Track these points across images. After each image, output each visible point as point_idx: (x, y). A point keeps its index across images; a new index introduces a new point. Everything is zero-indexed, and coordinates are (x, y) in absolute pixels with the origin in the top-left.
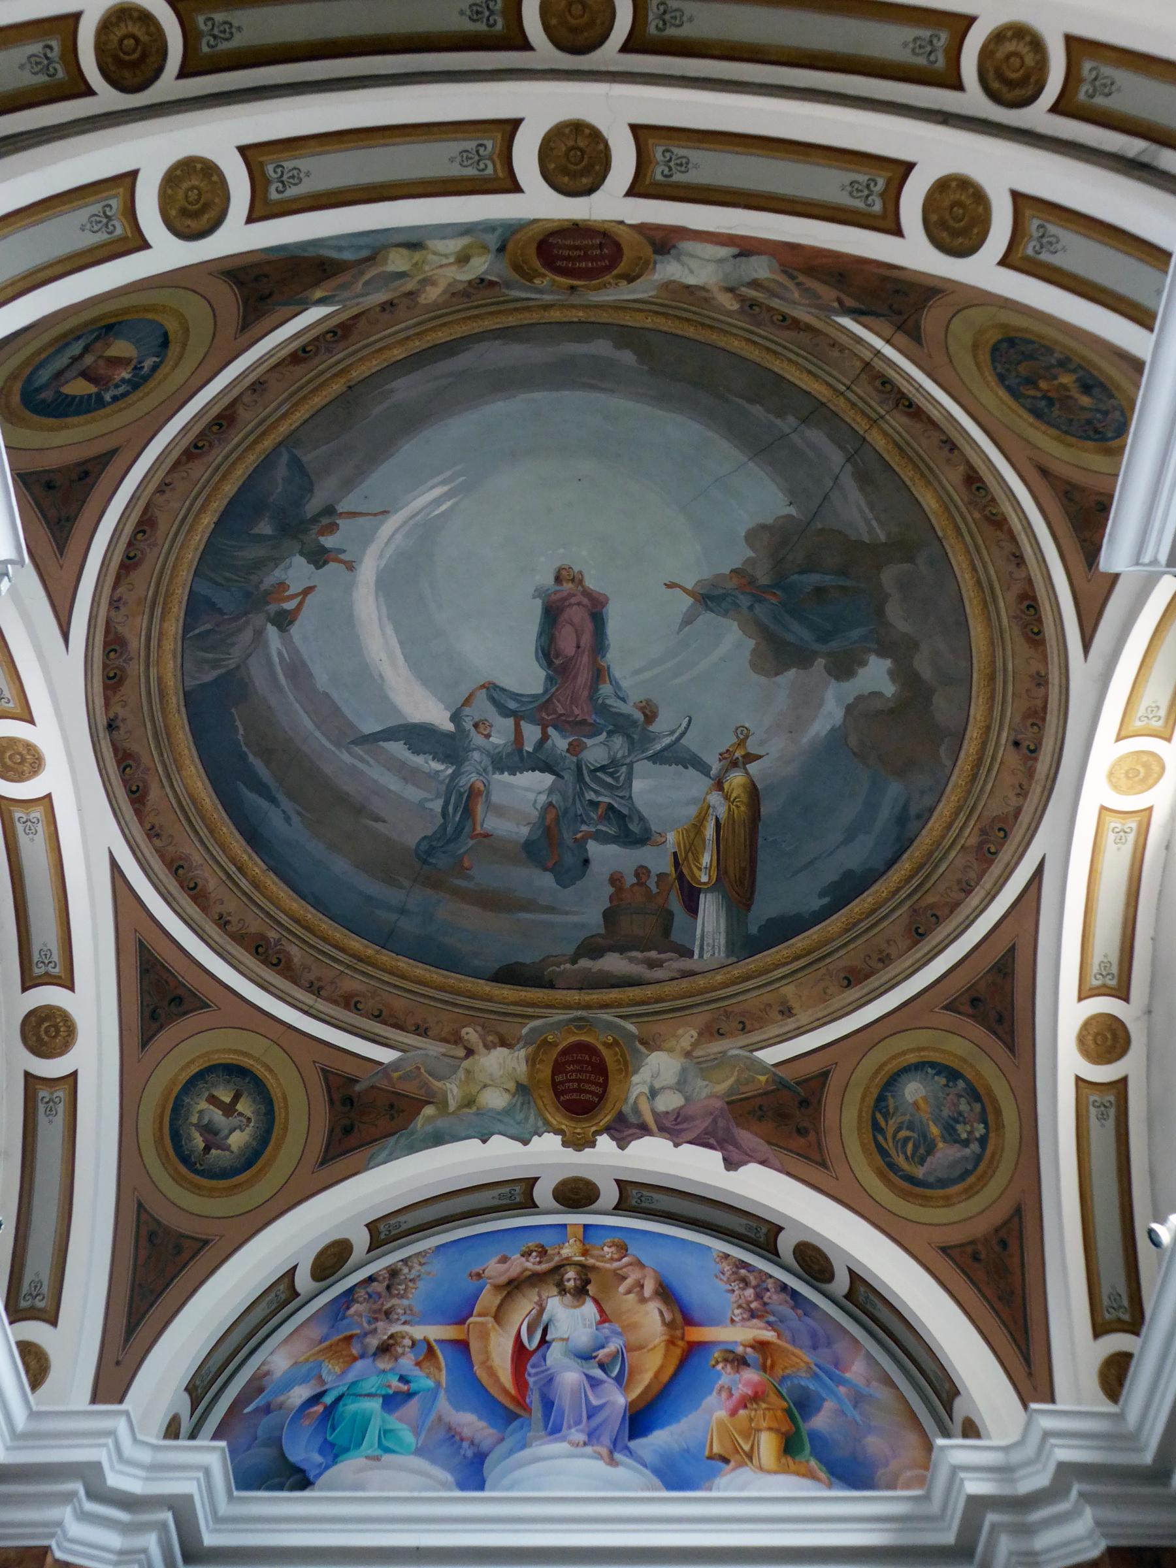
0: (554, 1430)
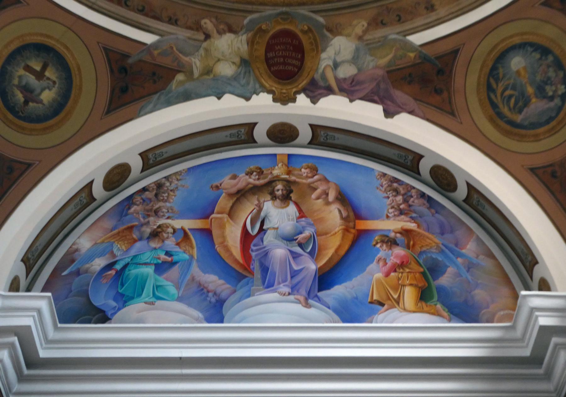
0: (269, 285)
